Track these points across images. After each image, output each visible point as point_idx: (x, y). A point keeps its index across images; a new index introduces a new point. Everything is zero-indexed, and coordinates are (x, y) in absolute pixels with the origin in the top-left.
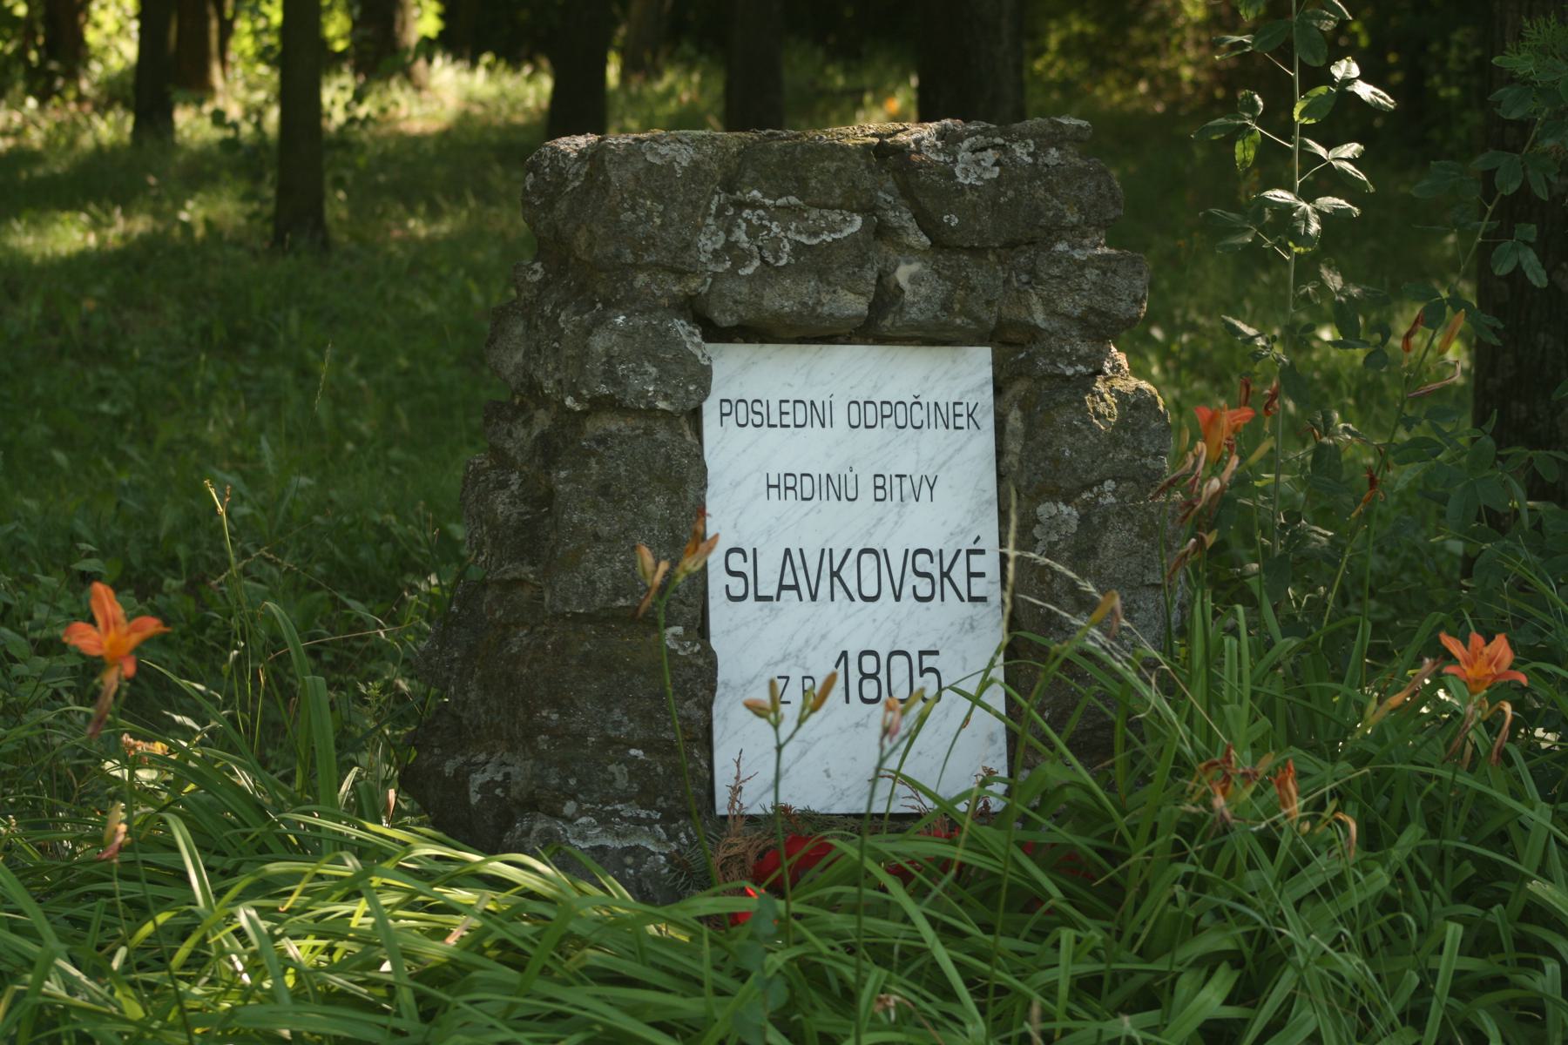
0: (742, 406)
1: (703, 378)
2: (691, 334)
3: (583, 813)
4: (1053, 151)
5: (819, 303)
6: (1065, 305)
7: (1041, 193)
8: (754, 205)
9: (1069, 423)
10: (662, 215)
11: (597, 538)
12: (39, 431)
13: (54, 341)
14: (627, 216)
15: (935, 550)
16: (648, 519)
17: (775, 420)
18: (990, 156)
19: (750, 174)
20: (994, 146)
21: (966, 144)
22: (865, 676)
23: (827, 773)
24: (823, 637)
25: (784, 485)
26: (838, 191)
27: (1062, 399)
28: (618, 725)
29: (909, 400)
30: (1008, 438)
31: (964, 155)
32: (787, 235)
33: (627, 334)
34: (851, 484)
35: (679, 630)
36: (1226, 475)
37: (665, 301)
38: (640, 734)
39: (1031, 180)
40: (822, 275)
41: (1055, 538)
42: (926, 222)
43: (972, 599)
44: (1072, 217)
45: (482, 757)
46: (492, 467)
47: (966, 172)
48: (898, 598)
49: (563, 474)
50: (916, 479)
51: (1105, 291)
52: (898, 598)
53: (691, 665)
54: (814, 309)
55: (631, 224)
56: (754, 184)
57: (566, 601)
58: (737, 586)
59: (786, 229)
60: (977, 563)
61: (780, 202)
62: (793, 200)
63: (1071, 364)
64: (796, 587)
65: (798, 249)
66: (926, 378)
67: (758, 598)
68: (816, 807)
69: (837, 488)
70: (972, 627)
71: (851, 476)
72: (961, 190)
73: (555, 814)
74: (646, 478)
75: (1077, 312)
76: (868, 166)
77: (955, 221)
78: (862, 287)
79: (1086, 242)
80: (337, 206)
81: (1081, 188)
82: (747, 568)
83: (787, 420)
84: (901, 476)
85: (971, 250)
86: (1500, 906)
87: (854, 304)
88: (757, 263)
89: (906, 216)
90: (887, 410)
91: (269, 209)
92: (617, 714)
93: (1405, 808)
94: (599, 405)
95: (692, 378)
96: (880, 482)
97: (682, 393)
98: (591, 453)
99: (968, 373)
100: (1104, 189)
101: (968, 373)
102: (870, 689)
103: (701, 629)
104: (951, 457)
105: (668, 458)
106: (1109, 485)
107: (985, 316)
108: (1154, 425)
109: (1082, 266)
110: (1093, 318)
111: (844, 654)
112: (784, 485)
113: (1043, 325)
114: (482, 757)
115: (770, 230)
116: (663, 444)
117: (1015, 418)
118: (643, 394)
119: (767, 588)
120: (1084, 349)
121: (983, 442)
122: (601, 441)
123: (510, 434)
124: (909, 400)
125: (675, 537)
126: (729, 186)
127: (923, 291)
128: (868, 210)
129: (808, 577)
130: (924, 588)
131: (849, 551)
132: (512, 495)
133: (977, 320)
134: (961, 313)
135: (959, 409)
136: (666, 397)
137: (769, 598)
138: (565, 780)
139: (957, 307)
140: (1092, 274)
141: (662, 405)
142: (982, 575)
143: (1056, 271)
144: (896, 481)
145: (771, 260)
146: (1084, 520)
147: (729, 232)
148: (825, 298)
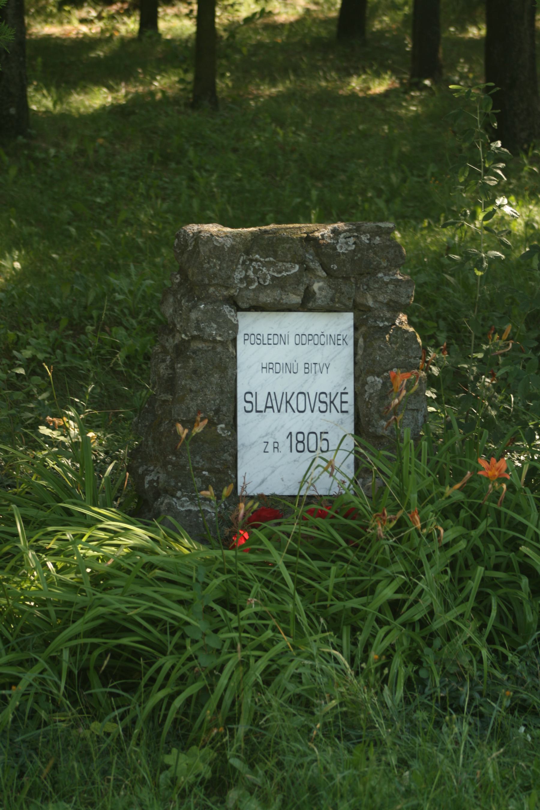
0: (253, 336)
1: (235, 328)
2: (231, 311)
3: (183, 496)
4: (378, 238)
5: (282, 299)
6: (381, 298)
7: (372, 255)
8: (257, 261)
9: (379, 347)
10: (220, 265)
11: (191, 391)
12: (66, 213)
13: (82, 160)
14: (206, 266)
15: (328, 393)
16: (211, 384)
17: (266, 342)
18: (352, 240)
19: (255, 248)
21: (342, 236)
22: (298, 442)
23: (282, 480)
24: (282, 427)
25: (269, 367)
27: (376, 336)
28: (198, 462)
29: (319, 334)
30: (359, 349)
31: (341, 239)
32: (269, 273)
33: (205, 312)
34: (295, 367)
35: (223, 426)
36: (401, 397)
37: (221, 298)
38: (207, 466)
39: (368, 250)
40: (282, 288)
41: (372, 391)
42: (324, 267)
43: (342, 412)
45: (152, 468)
46: (161, 352)
47: (341, 247)
48: (312, 411)
49: (179, 365)
50: (321, 365)
51: (396, 293)
52: (312, 411)
55: (208, 269)
56: (257, 253)
57: (179, 415)
58: (249, 407)
59: (269, 270)
60: (345, 398)
61: (267, 260)
62: (272, 259)
63: (383, 321)
64: (272, 407)
65: (273, 278)
66: (327, 325)
67: (257, 411)
68: (278, 493)
69: (289, 368)
70: (342, 423)
71: (295, 364)
72: (339, 255)
73: (173, 496)
74: (211, 367)
75: (385, 301)
76: (302, 246)
77: (336, 267)
78: (298, 293)
80: (224, 84)
82: (253, 400)
86: (483, 569)
87: (296, 299)
88: (256, 284)
89: (317, 264)
90: (310, 338)
91: (190, 87)
92: (198, 458)
93: (296, 619)
94: (194, 338)
95: (230, 329)
96: (307, 366)
97: (226, 334)
98: (190, 357)
99: (344, 323)
100: (397, 253)
101: (344, 323)
102: (300, 447)
103: (233, 426)
105: (221, 359)
108: (414, 346)
109: (387, 284)
110: (391, 303)
111: (290, 433)
112: (269, 367)
114: (152, 468)
116: (219, 353)
117: (361, 341)
118: (211, 335)
119: (261, 407)
120: (388, 315)
121: (349, 350)
122: (194, 352)
123: (167, 340)
124: (319, 334)
125: (222, 390)
126: (248, 252)
127: (324, 293)
128: (301, 263)
129: (274, 404)
130: (323, 408)
132: (167, 366)
134: (338, 302)
135: (339, 337)
136: (220, 336)
137: (261, 412)
138: (177, 483)
140: (391, 287)
141: (218, 338)
142: (346, 402)
143: (376, 286)
146: (384, 384)
147: (246, 271)
148: (284, 297)
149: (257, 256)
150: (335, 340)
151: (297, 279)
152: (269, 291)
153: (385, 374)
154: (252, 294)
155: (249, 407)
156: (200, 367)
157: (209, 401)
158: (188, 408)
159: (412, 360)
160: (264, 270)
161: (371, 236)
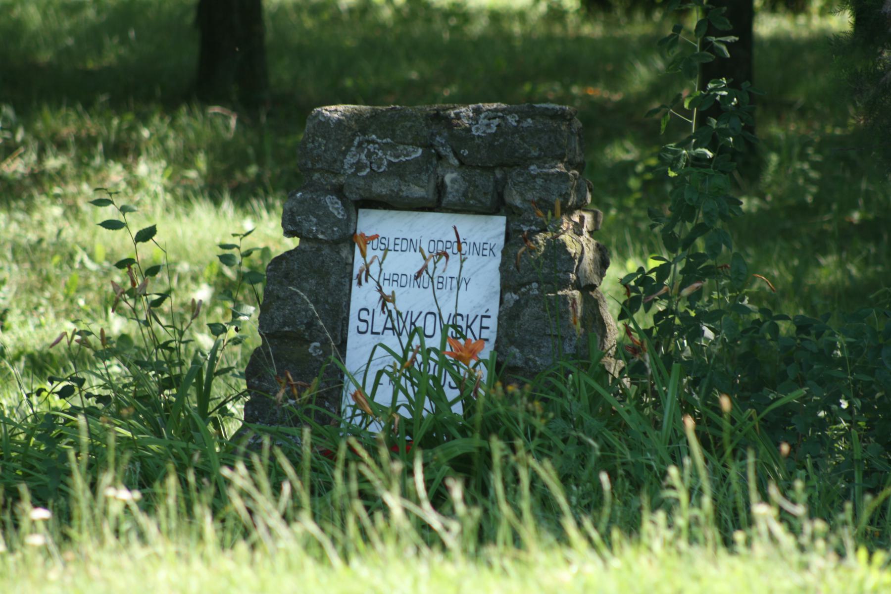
4: (529, 120)
5: (400, 190)
6: (529, 196)
7: (518, 140)
8: (373, 142)
10: (325, 145)
11: (278, 298)
14: (310, 145)
15: (464, 314)
17: (391, 247)
20: (499, 117)
26: (410, 137)
31: (483, 121)
33: (302, 202)
35: (317, 344)
37: (329, 187)
39: (513, 134)
40: (401, 177)
42: (456, 154)
44: (535, 153)
51: (546, 189)
53: (317, 361)
54: (398, 193)
55: (312, 149)
56: (373, 133)
58: (363, 327)
59: (385, 154)
60: (486, 323)
61: (384, 141)
62: (389, 140)
65: (390, 164)
66: (471, 230)
67: (373, 333)
76: (427, 125)
79: (547, 165)
81: (540, 139)
82: (369, 319)
83: (397, 248)
84: (452, 278)
85: (333, 173)
97: (329, 231)
99: (490, 230)
101: (490, 230)
104: (478, 270)
105: (323, 262)
106: (535, 285)
107: (483, 200)
108: (563, 257)
109: (534, 177)
110: (541, 203)
113: (520, 206)
115: (377, 154)
118: (311, 231)
121: (497, 261)
128: (428, 146)
131: (421, 313)
133: (480, 202)
134: (472, 198)
135: (485, 246)
136: (322, 233)
137: (378, 333)
139: (470, 195)
142: (487, 328)
143: (521, 179)
144: (449, 280)
145: (375, 169)
148: (404, 188)
149: (374, 136)
150: (480, 250)
151: (420, 166)
152: (383, 180)
153: (523, 290)
154: (362, 182)
155: (363, 327)
156: (293, 270)
157: (299, 312)
158: (272, 319)
159: (561, 275)
160: (380, 153)
161: (520, 118)
